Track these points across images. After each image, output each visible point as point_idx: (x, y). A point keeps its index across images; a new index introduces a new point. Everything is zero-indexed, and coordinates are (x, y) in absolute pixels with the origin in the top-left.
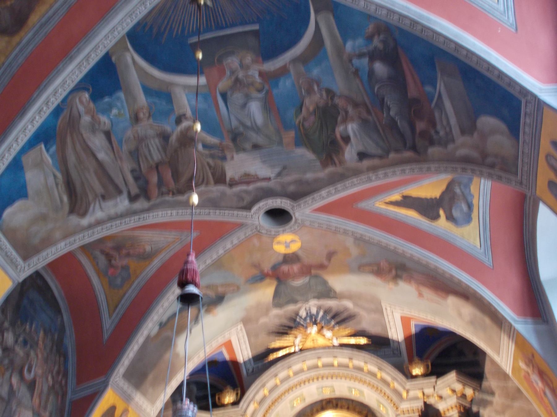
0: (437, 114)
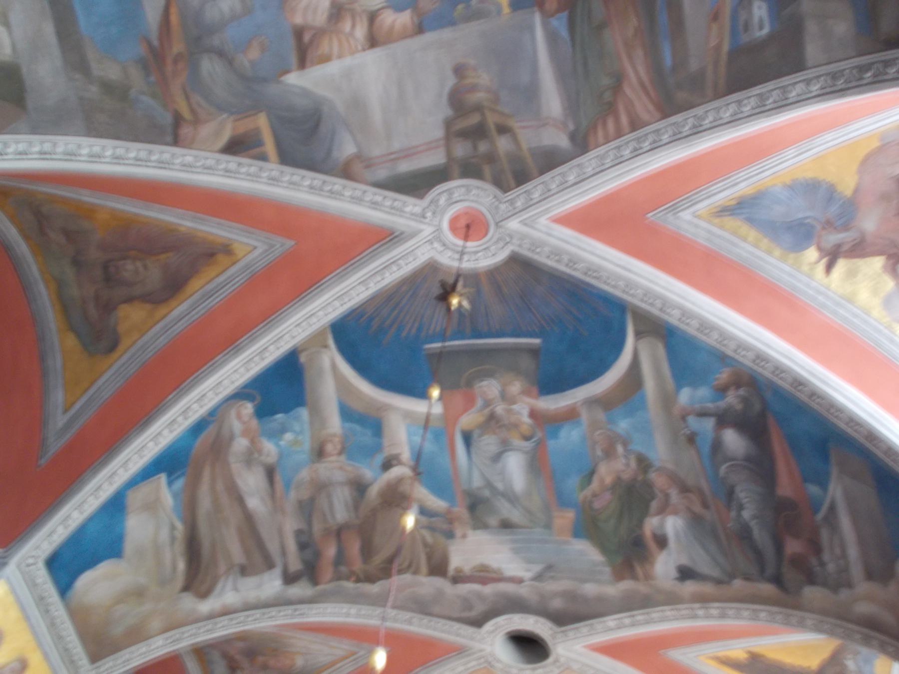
0: (825, 534)
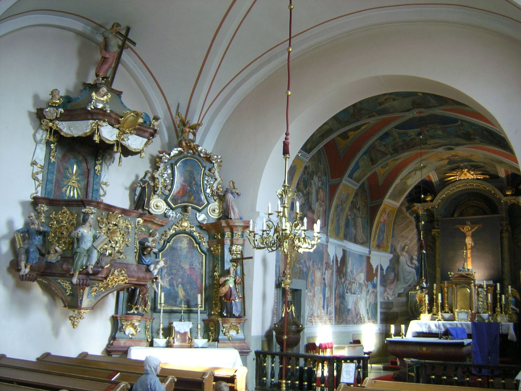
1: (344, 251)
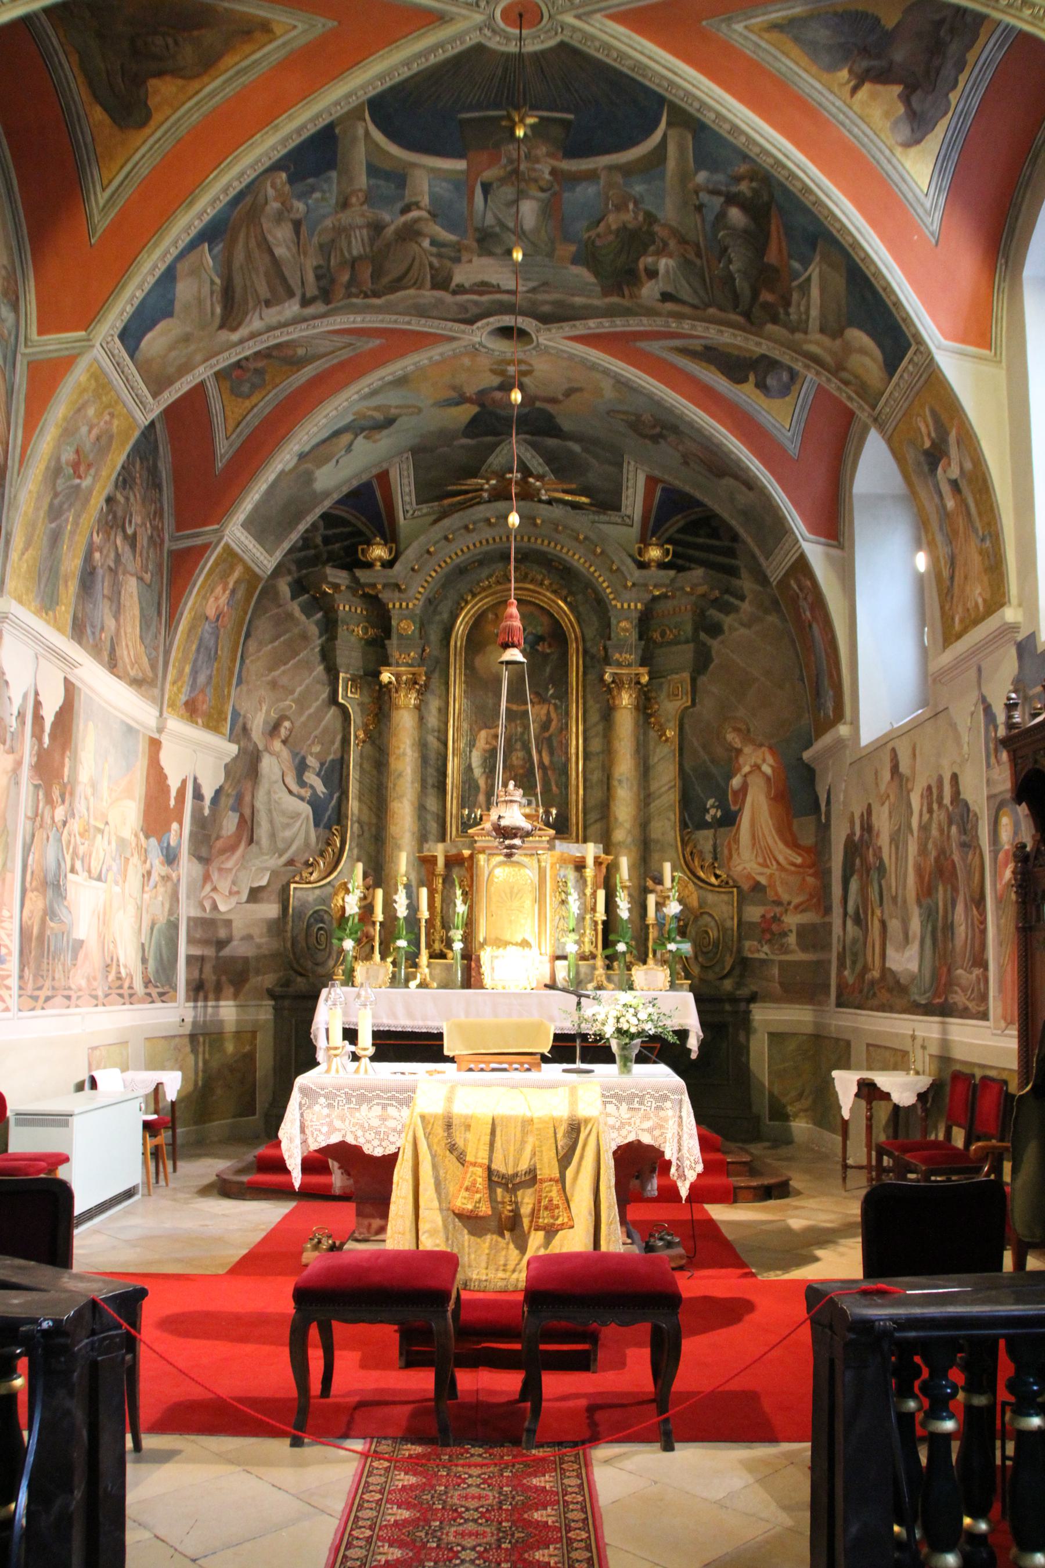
0: (795, 296)
1: (70, 688)
